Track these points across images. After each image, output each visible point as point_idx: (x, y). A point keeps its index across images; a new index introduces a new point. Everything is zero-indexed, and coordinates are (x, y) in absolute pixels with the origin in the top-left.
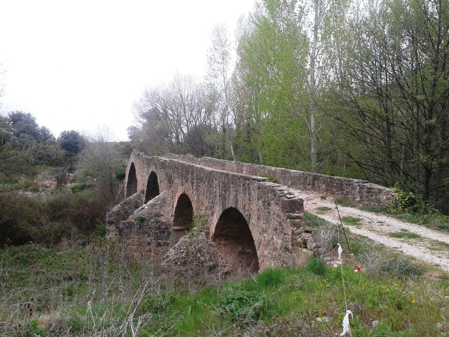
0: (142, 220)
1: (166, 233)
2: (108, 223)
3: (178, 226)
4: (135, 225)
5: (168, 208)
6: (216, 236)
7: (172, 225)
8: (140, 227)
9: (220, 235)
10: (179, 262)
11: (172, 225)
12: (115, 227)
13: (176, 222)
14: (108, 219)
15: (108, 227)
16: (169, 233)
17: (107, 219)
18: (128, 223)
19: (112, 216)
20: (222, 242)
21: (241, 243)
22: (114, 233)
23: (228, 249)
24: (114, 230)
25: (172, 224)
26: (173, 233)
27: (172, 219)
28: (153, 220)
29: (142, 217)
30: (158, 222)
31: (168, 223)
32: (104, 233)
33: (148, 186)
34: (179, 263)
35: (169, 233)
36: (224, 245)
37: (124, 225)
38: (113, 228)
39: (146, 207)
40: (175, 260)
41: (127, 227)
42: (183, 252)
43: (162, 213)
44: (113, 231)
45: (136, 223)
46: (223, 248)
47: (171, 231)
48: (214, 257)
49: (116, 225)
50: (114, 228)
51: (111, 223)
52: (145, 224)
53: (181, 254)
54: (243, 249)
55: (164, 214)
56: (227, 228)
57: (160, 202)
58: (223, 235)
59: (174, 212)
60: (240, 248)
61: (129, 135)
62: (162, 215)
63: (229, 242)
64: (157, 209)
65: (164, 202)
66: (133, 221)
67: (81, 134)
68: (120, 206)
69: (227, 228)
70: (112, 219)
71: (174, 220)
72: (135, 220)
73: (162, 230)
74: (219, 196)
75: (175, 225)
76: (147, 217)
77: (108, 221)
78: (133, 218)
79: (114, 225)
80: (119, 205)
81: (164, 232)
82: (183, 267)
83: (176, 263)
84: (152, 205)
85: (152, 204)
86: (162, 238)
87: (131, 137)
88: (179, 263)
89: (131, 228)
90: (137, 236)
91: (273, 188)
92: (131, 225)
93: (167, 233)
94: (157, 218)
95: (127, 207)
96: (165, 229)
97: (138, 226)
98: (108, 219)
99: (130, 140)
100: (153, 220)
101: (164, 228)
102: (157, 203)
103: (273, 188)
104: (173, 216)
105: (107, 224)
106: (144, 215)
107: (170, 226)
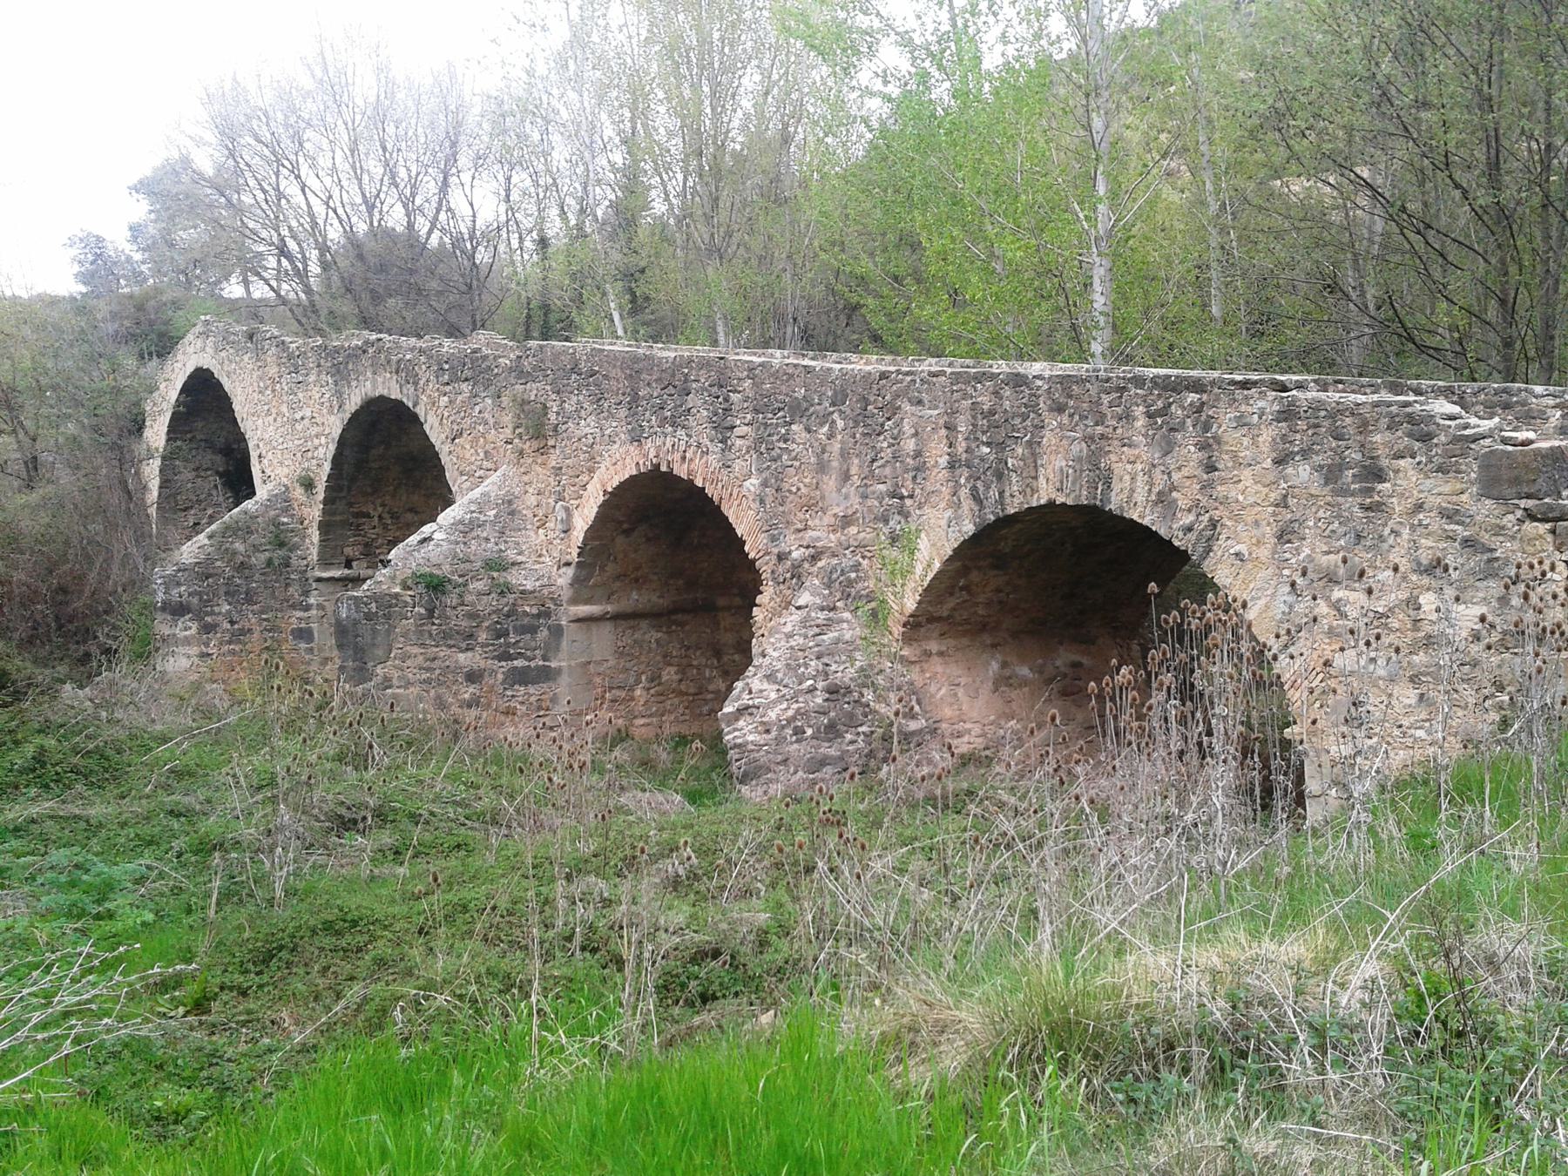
0: (435, 586)
1: (543, 633)
2: (163, 609)
3: (587, 602)
4: (406, 604)
5: (532, 534)
6: (915, 625)
7: (565, 598)
8: (431, 612)
9: (932, 620)
10: (809, 726)
11: (565, 598)
12: (194, 627)
13: (582, 587)
14: (161, 594)
15: (162, 627)
16: (557, 632)
17: (160, 597)
18: (375, 598)
19: (179, 584)
20: (934, 646)
21: (994, 646)
22: (194, 650)
23: (955, 670)
24: (193, 636)
25: (566, 594)
26: (571, 632)
27: (564, 578)
28: (479, 585)
29: (431, 575)
30: (505, 590)
31: (545, 592)
32: (146, 650)
33: (337, 461)
34: (809, 732)
35: (557, 632)
36: (941, 654)
37: (357, 607)
38: (187, 628)
39: (437, 536)
40: (794, 718)
41: (369, 617)
42: (812, 690)
43: (511, 554)
44: (187, 641)
45: (409, 599)
46: (939, 669)
47: (563, 623)
48: (919, 702)
49: (199, 617)
50: (193, 631)
51: (178, 610)
52: (452, 599)
53: (809, 695)
54: (1004, 665)
55: (520, 558)
56: (962, 589)
57: (494, 512)
58: (939, 619)
59: (575, 552)
60: (995, 666)
61: (76, 268)
62: (513, 564)
63: (952, 642)
64: (487, 540)
65: (512, 513)
66: (397, 590)
67: (149, 173)
68: (206, 541)
69: (962, 589)
70: (180, 592)
71: (576, 582)
72: (406, 587)
73: (526, 621)
74: (952, 466)
75: (574, 601)
76: (453, 573)
77: (164, 602)
78: (393, 578)
79: (190, 620)
80: (202, 538)
81: (533, 630)
82: (827, 744)
83: (799, 731)
84: (461, 527)
85: (461, 522)
86: (528, 653)
87: (85, 278)
88: (809, 732)
89: (388, 617)
90: (416, 650)
91: (1409, 410)
92: (387, 606)
93: (546, 632)
94: (495, 574)
95: (239, 546)
96: (539, 616)
97: (422, 611)
98: (161, 594)
99: (84, 289)
100: (479, 585)
101: (535, 611)
102: (482, 518)
103: (1409, 410)
104: (568, 564)
105: (159, 616)
106: (439, 566)
107: (557, 602)
